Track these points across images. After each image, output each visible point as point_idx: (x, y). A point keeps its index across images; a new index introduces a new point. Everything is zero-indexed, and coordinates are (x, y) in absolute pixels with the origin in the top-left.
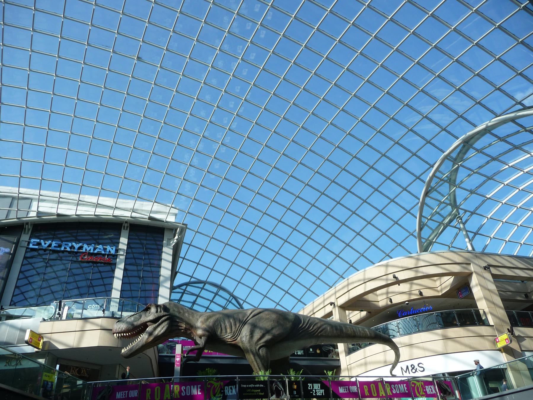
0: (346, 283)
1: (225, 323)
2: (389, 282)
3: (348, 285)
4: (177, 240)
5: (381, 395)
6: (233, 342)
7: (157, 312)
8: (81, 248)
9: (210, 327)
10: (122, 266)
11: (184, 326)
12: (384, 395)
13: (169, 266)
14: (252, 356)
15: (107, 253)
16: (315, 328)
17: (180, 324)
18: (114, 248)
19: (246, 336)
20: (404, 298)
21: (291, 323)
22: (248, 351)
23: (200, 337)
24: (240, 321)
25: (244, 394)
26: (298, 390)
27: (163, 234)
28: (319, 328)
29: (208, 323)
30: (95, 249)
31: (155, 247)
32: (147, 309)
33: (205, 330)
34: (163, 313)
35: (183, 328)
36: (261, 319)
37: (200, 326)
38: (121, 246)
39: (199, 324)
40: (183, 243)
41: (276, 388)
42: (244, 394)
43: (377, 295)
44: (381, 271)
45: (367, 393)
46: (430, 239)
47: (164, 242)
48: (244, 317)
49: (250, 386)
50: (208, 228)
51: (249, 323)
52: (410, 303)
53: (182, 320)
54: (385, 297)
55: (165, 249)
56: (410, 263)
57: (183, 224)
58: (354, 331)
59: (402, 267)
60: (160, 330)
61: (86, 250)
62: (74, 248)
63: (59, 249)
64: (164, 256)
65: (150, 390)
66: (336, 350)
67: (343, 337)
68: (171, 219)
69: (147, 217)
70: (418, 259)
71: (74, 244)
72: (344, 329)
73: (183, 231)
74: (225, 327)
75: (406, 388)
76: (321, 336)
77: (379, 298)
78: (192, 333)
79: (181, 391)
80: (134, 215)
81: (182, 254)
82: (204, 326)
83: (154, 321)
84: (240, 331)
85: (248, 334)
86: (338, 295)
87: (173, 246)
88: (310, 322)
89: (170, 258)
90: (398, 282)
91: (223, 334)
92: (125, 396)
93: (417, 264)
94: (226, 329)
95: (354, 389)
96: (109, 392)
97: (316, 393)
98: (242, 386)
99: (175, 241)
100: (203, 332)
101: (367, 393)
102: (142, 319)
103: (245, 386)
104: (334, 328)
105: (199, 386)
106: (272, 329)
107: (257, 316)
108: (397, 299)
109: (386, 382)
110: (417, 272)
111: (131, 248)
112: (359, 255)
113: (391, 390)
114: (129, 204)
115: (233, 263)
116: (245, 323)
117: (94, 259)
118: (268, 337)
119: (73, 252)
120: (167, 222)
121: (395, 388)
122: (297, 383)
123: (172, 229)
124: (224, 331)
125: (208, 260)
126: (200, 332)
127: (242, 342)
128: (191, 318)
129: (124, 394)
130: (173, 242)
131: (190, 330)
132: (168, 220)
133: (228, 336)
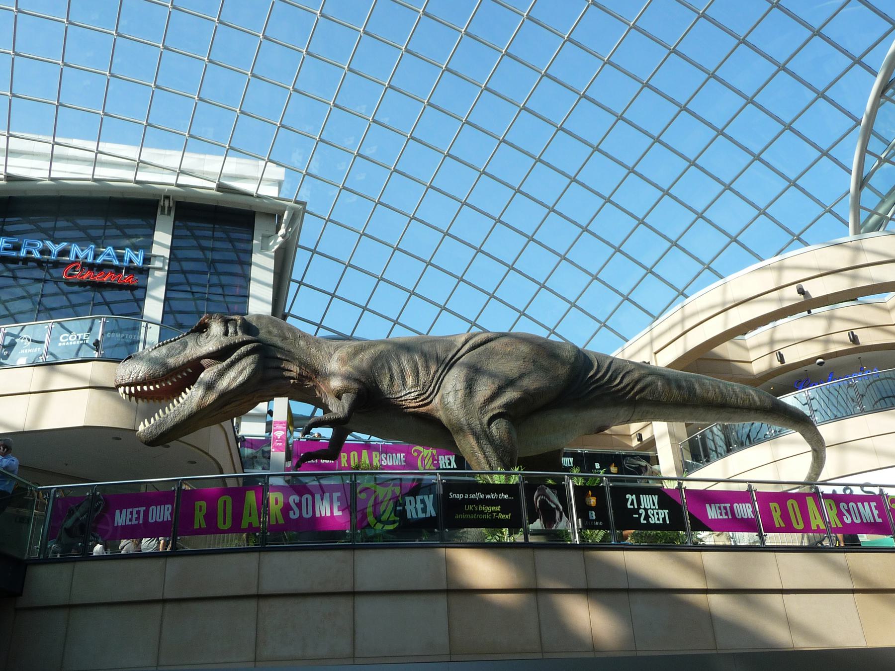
0: (678, 316)
1: (400, 364)
2: (786, 304)
3: (683, 320)
4: (283, 236)
5: (814, 527)
6: (421, 410)
7: (226, 333)
8: (64, 252)
9: (362, 372)
10: (160, 292)
11: (294, 370)
12: (822, 527)
13: (268, 294)
14: (472, 440)
15: (126, 264)
16: (625, 382)
17: (284, 365)
18: (141, 254)
19: (456, 392)
20: (813, 351)
21: (568, 367)
22: (460, 430)
23: (339, 397)
24: (438, 361)
25: (457, 517)
26: (601, 509)
27: (250, 227)
28: (637, 382)
29: (356, 362)
30: (96, 256)
31: (232, 256)
32: (202, 328)
33: (348, 377)
34: (241, 336)
35: (293, 374)
36: (492, 353)
37: (337, 369)
38: (156, 250)
39: (334, 365)
40: (298, 246)
41: (543, 502)
42: (457, 517)
43: (747, 349)
44: (768, 280)
45: (778, 521)
46: (881, 211)
47: (255, 242)
48: (448, 350)
49: (472, 496)
50: (352, 210)
51: (462, 364)
52: (827, 362)
53: (291, 357)
54: (766, 350)
55: (256, 258)
56: (839, 258)
57: (296, 202)
58: (722, 394)
59: (820, 269)
60: (237, 375)
61: (77, 257)
62: (49, 252)
63: (14, 254)
64: (255, 272)
65: (203, 504)
66: (655, 467)
67: (695, 406)
68: (269, 191)
69: (214, 185)
70: (858, 249)
71: (49, 244)
72: (697, 386)
73: (296, 217)
74: (402, 371)
75: (876, 512)
76: (643, 401)
77: (752, 356)
78: (316, 386)
79: (286, 508)
80: (184, 180)
81: (296, 274)
82: (347, 369)
83: (219, 355)
84: (440, 381)
85: (460, 386)
86: (657, 346)
87: (276, 252)
88: (613, 368)
89: (270, 278)
90: (807, 305)
91: (396, 388)
92: (138, 519)
93: (854, 259)
94: (403, 378)
95: (745, 510)
96: (96, 510)
97: (647, 517)
98: (452, 496)
99: (280, 239)
100: (346, 383)
101: (778, 521)
102: (188, 351)
103: (459, 496)
104: (674, 385)
105: (336, 495)
106: (522, 376)
107: (482, 348)
108: (793, 356)
109: (826, 496)
110: (854, 277)
111: (179, 260)
112: (701, 267)
113: (840, 515)
114: (172, 158)
115: (412, 293)
116: (449, 365)
117: (98, 277)
118: (510, 395)
119: (48, 262)
120: (259, 197)
121: (848, 511)
122: (598, 491)
123: (273, 215)
124: (398, 381)
125: (356, 287)
126: (336, 383)
127: (445, 406)
128: (313, 350)
129: (135, 516)
130: (275, 244)
131: (310, 379)
132: (261, 192)
133: (407, 394)
